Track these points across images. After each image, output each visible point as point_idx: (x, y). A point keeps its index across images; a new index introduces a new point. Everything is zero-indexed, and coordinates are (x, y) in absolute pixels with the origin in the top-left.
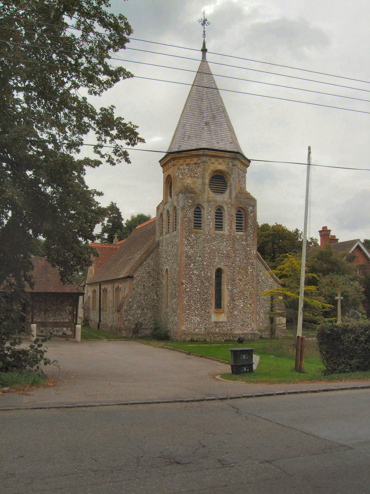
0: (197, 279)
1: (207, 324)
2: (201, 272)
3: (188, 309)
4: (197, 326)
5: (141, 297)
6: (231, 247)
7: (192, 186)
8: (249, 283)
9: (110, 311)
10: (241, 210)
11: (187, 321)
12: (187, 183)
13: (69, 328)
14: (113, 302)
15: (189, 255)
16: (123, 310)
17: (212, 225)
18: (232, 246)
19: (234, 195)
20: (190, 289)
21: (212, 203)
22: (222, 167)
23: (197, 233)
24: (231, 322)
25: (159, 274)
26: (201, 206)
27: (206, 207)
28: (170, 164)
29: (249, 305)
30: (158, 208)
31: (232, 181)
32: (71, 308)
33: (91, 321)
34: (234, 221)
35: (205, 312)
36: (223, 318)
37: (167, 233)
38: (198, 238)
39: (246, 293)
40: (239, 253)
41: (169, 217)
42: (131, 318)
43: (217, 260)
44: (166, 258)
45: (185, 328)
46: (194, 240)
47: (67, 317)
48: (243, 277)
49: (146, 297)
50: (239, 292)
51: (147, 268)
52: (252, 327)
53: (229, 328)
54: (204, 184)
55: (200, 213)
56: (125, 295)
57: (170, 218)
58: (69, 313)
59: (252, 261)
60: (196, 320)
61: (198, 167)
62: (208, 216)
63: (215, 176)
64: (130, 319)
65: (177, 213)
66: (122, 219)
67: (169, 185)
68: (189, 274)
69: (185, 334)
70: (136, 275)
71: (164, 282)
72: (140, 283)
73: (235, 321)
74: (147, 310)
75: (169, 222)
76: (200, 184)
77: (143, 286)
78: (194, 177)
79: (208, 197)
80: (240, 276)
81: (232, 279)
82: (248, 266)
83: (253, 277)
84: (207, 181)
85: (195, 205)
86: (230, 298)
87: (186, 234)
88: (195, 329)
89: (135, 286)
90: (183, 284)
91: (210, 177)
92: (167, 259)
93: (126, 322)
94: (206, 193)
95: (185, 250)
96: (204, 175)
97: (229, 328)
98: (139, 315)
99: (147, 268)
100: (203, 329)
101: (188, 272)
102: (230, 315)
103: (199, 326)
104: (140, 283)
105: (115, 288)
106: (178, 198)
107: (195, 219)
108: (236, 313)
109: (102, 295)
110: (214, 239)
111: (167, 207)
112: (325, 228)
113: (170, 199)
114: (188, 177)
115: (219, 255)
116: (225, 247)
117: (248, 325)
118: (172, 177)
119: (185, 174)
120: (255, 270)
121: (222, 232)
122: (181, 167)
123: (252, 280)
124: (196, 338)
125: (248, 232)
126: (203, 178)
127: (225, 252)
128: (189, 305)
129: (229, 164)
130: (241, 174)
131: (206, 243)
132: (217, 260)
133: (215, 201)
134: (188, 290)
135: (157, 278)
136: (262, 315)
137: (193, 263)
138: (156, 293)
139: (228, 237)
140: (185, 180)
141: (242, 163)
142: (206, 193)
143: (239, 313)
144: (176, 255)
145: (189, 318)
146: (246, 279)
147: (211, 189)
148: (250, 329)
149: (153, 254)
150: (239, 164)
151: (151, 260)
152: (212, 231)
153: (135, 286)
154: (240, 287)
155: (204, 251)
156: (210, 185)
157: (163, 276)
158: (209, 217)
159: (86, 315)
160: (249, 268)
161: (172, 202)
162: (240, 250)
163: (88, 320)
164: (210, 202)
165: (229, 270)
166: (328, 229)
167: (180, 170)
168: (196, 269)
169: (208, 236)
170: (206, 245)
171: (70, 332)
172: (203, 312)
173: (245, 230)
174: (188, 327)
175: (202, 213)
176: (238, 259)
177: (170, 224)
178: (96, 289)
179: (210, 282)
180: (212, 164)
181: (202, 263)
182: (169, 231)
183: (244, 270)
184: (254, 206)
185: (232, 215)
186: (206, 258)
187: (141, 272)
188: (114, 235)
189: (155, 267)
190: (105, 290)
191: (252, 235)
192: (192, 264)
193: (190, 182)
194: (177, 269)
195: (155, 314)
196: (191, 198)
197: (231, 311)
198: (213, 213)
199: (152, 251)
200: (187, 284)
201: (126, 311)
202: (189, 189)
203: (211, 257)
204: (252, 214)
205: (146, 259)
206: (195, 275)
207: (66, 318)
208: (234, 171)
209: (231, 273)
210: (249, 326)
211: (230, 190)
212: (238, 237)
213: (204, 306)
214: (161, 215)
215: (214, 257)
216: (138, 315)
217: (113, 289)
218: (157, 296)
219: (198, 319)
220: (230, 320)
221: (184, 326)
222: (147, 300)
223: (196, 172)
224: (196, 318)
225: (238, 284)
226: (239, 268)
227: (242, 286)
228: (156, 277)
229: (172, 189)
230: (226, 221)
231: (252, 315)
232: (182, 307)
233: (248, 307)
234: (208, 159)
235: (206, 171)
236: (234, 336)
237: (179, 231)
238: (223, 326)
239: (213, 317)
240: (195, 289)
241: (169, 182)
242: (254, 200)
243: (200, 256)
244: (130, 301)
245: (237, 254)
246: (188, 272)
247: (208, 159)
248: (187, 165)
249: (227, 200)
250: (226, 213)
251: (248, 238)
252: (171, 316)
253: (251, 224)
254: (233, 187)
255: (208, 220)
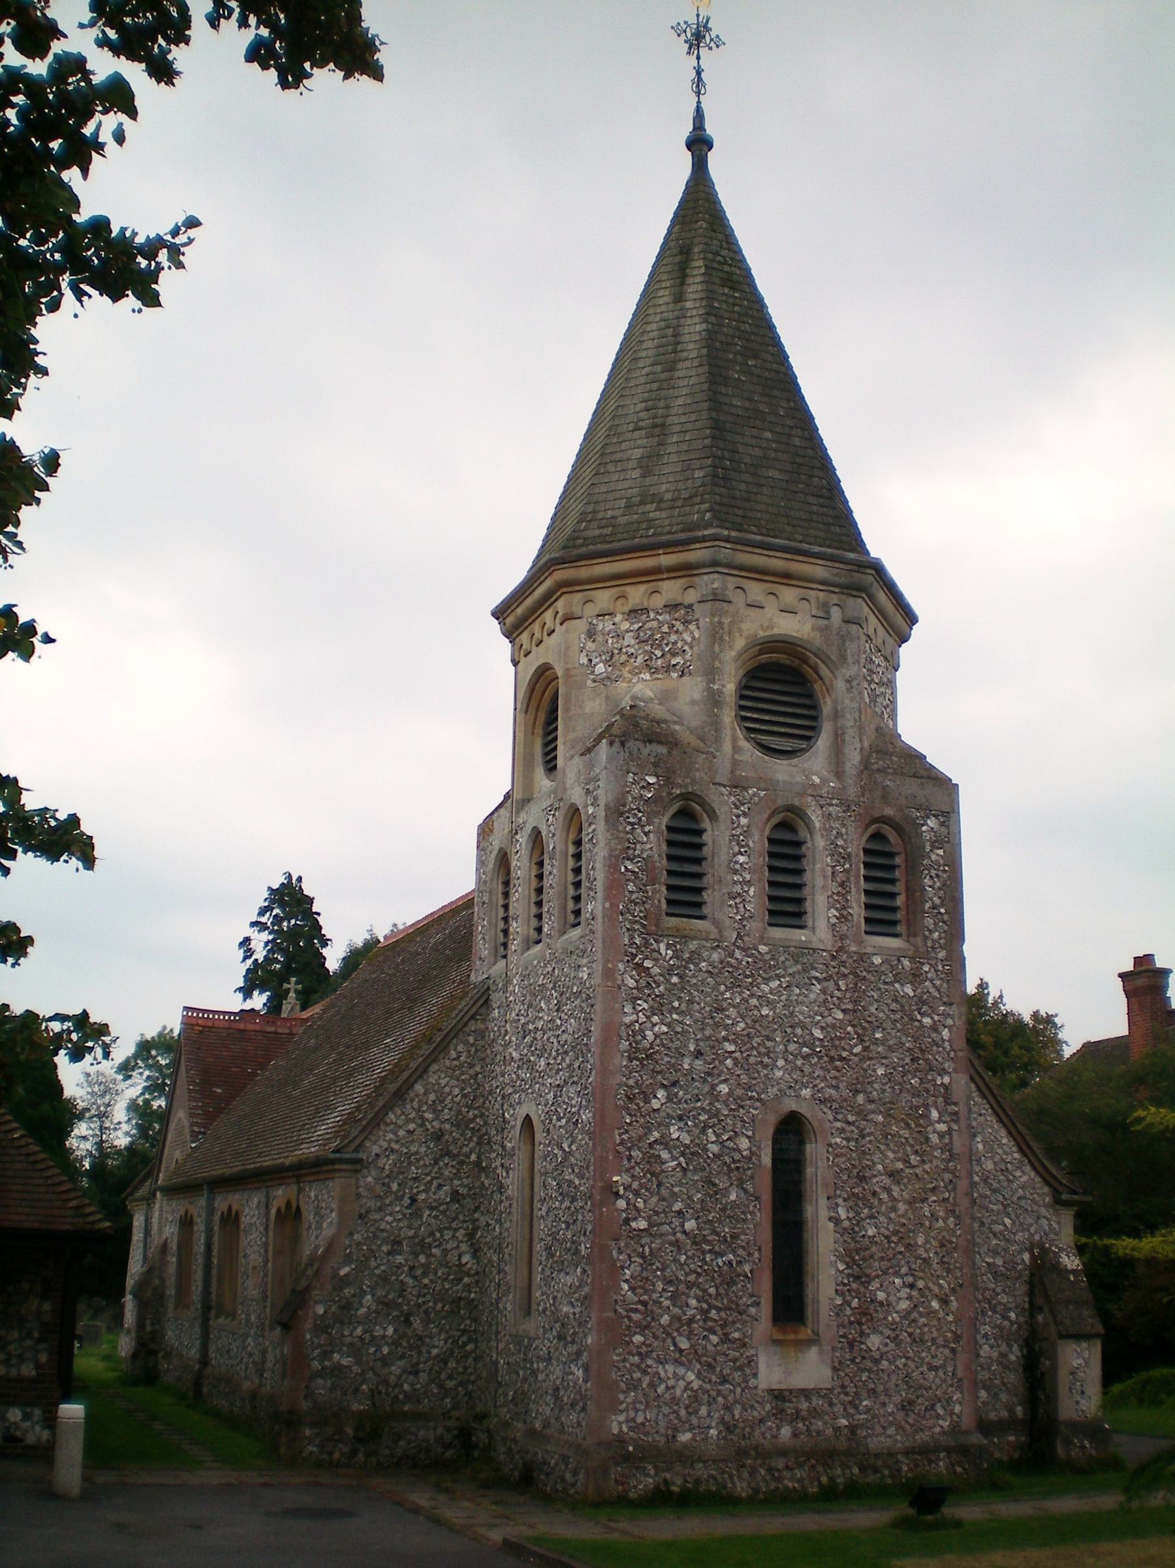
0: (684, 1170)
1: (736, 1401)
2: (703, 1132)
3: (638, 1324)
4: (683, 1412)
5: (399, 1259)
6: (844, 1011)
7: (658, 710)
8: (933, 1190)
9: (248, 1321)
10: (887, 830)
11: (634, 1386)
12: (634, 698)
13: (37, 1412)
14: (266, 1275)
15: (646, 1044)
16: (309, 1325)
17: (755, 896)
18: (850, 1006)
19: (853, 757)
20: (648, 1219)
21: (755, 795)
22: (796, 626)
23: (686, 938)
24: (851, 1389)
25: (484, 1141)
26: (703, 803)
27: (726, 808)
28: (548, 616)
29: (935, 1304)
30: (486, 829)
31: (838, 693)
32: (47, 1306)
33: (168, 1355)
34: (858, 880)
35: (726, 1339)
36: (811, 1370)
37: (528, 944)
38: (690, 960)
39: (920, 1241)
40: (883, 1042)
41: (541, 864)
42: (345, 1362)
43: (779, 1074)
44: (525, 1062)
45: (625, 1429)
46: (670, 970)
47: (29, 1355)
48: (906, 1161)
49: (422, 1259)
50: (887, 1237)
51: (429, 1116)
52: (952, 1413)
53: (844, 1422)
54: (714, 699)
55: (695, 839)
56: (317, 1247)
57: (547, 868)
58: (36, 1334)
59: (946, 1080)
60: (682, 1384)
61: (686, 623)
62: (735, 855)
63: (762, 667)
64: (339, 1366)
65: (585, 839)
66: (325, 942)
67: (542, 717)
68: (644, 1145)
69: (627, 1458)
70: (375, 1149)
71: (513, 1182)
72: (395, 1187)
73: (871, 1386)
74: (426, 1322)
75: (539, 891)
76: (693, 702)
77: (407, 1201)
78: (669, 668)
79: (735, 764)
80: (891, 1155)
81: (855, 1172)
82: (926, 1106)
83: (952, 1157)
84: (730, 687)
85: (674, 799)
86: (848, 1267)
87: (632, 937)
88: (675, 1429)
89: (371, 1204)
90: (617, 1195)
91: (741, 672)
92: (532, 1066)
93: (320, 1381)
94: (727, 747)
95: (627, 1020)
96: (715, 656)
97: (844, 1422)
98: (385, 1350)
99: (429, 1116)
100: (713, 1432)
101: (641, 1131)
102: (848, 1356)
103: (696, 1412)
104: (395, 1187)
105: (273, 1212)
106: (591, 766)
107: (675, 867)
108: (874, 1341)
109: (216, 1239)
110: (765, 968)
111: (532, 817)
112: (1143, 962)
113: (543, 782)
114: (636, 672)
115: (792, 1047)
116: (813, 1008)
117: (933, 1407)
118: (560, 673)
119: (624, 658)
120: (963, 1123)
121: (802, 936)
122: (606, 625)
123: (947, 1176)
124: (679, 1481)
125: (925, 938)
126: (711, 673)
127: (818, 1033)
128: (644, 1304)
129: (828, 612)
130: (880, 670)
131: (728, 989)
132: (779, 1074)
133: (768, 784)
134: (643, 1224)
135: (478, 1164)
136: (986, 1348)
137: (663, 1086)
138: (471, 1235)
139: (833, 958)
140: (622, 685)
141: (882, 614)
142: (727, 747)
143: (892, 1345)
144: (579, 1048)
145: (644, 1372)
146: (919, 1171)
147: (749, 729)
148: (946, 1424)
149: (460, 1048)
150: (873, 620)
151: (451, 1077)
152: (753, 926)
153: (371, 1204)
154: (894, 1209)
155: (717, 1025)
156: (742, 708)
157: (506, 1154)
158: (741, 859)
159: (149, 1329)
160: (935, 1114)
161: (559, 794)
162: (888, 1025)
163: (155, 1353)
164: (745, 789)
165: (839, 1125)
166: (1160, 963)
167: (600, 638)
168: (680, 1118)
169: (738, 954)
170: (728, 995)
171: (38, 1428)
172: (714, 1339)
173: (909, 924)
174: (640, 1419)
175: (706, 837)
176: (880, 1071)
177: (549, 894)
178: (194, 1211)
179: (749, 1186)
180: (753, 612)
181: (707, 1088)
182: (539, 930)
183: (907, 1125)
184: (948, 814)
185: (849, 855)
186: (729, 1062)
187: (401, 1133)
188: (286, 986)
189: (470, 1107)
190: (231, 1219)
191: (942, 954)
192: (661, 1094)
193: (649, 694)
194: (586, 1116)
195: (465, 1344)
196: (657, 765)
197: (853, 1333)
198: (758, 842)
199: (457, 1032)
200: (637, 1193)
201: (322, 1327)
202: (644, 724)
203: (752, 1060)
204: (941, 852)
205: (426, 1071)
206: (675, 1147)
207: (22, 1359)
208: (851, 648)
209: (848, 1140)
210: (940, 1411)
211: (836, 735)
212: (877, 960)
213: (719, 1309)
214: (504, 860)
215: (766, 1060)
216: (379, 1349)
217: (267, 1214)
218: (476, 1253)
219: (691, 1376)
220: (847, 1382)
221: (622, 1418)
222: (425, 1274)
223: (675, 643)
224: (681, 1371)
225: (884, 1196)
226: (887, 1115)
227: (902, 1207)
228: (473, 1157)
229: (560, 732)
230: (819, 882)
231: (953, 1351)
232: (611, 1314)
233: (931, 1313)
234: (732, 582)
235: (721, 639)
236: (868, 1460)
237: (598, 925)
238: (814, 1413)
239: (763, 1361)
240: (676, 1222)
241: (541, 708)
242: (946, 787)
243: (698, 1054)
244: (341, 1279)
245: (876, 1042)
246: (641, 1131)
247: (731, 586)
248: (633, 613)
249: (824, 781)
250: (821, 843)
251: (926, 968)
252: (549, 1359)
253: (937, 900)
254: (849, 721)
255: (735, 872)
